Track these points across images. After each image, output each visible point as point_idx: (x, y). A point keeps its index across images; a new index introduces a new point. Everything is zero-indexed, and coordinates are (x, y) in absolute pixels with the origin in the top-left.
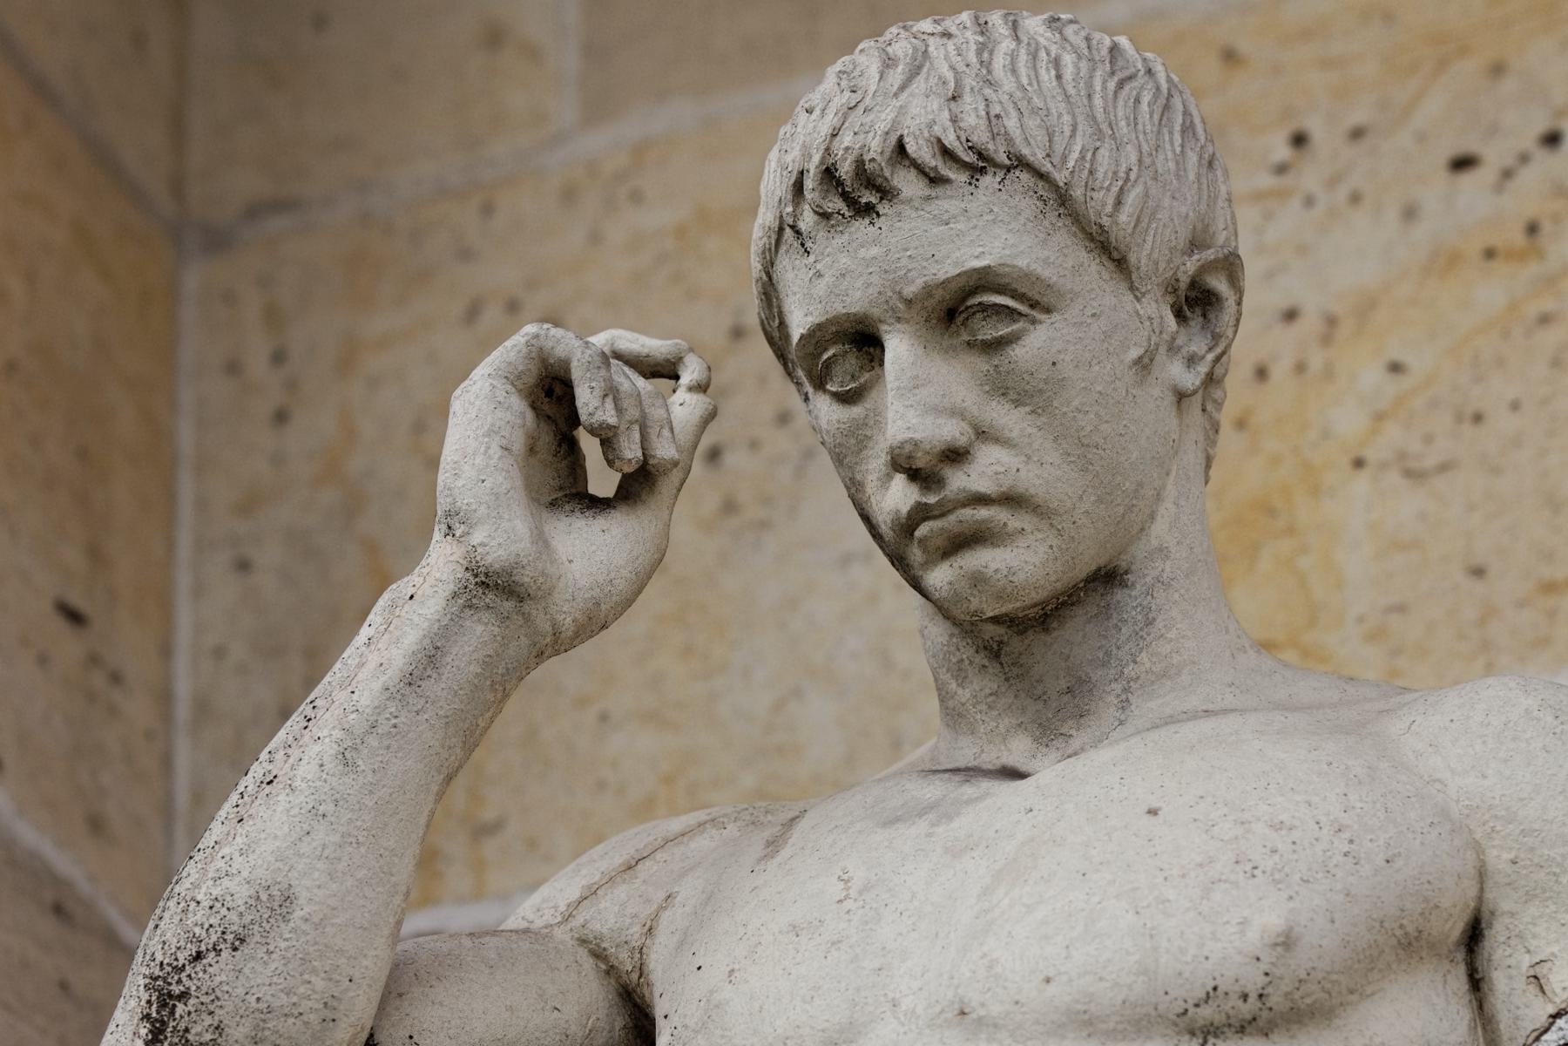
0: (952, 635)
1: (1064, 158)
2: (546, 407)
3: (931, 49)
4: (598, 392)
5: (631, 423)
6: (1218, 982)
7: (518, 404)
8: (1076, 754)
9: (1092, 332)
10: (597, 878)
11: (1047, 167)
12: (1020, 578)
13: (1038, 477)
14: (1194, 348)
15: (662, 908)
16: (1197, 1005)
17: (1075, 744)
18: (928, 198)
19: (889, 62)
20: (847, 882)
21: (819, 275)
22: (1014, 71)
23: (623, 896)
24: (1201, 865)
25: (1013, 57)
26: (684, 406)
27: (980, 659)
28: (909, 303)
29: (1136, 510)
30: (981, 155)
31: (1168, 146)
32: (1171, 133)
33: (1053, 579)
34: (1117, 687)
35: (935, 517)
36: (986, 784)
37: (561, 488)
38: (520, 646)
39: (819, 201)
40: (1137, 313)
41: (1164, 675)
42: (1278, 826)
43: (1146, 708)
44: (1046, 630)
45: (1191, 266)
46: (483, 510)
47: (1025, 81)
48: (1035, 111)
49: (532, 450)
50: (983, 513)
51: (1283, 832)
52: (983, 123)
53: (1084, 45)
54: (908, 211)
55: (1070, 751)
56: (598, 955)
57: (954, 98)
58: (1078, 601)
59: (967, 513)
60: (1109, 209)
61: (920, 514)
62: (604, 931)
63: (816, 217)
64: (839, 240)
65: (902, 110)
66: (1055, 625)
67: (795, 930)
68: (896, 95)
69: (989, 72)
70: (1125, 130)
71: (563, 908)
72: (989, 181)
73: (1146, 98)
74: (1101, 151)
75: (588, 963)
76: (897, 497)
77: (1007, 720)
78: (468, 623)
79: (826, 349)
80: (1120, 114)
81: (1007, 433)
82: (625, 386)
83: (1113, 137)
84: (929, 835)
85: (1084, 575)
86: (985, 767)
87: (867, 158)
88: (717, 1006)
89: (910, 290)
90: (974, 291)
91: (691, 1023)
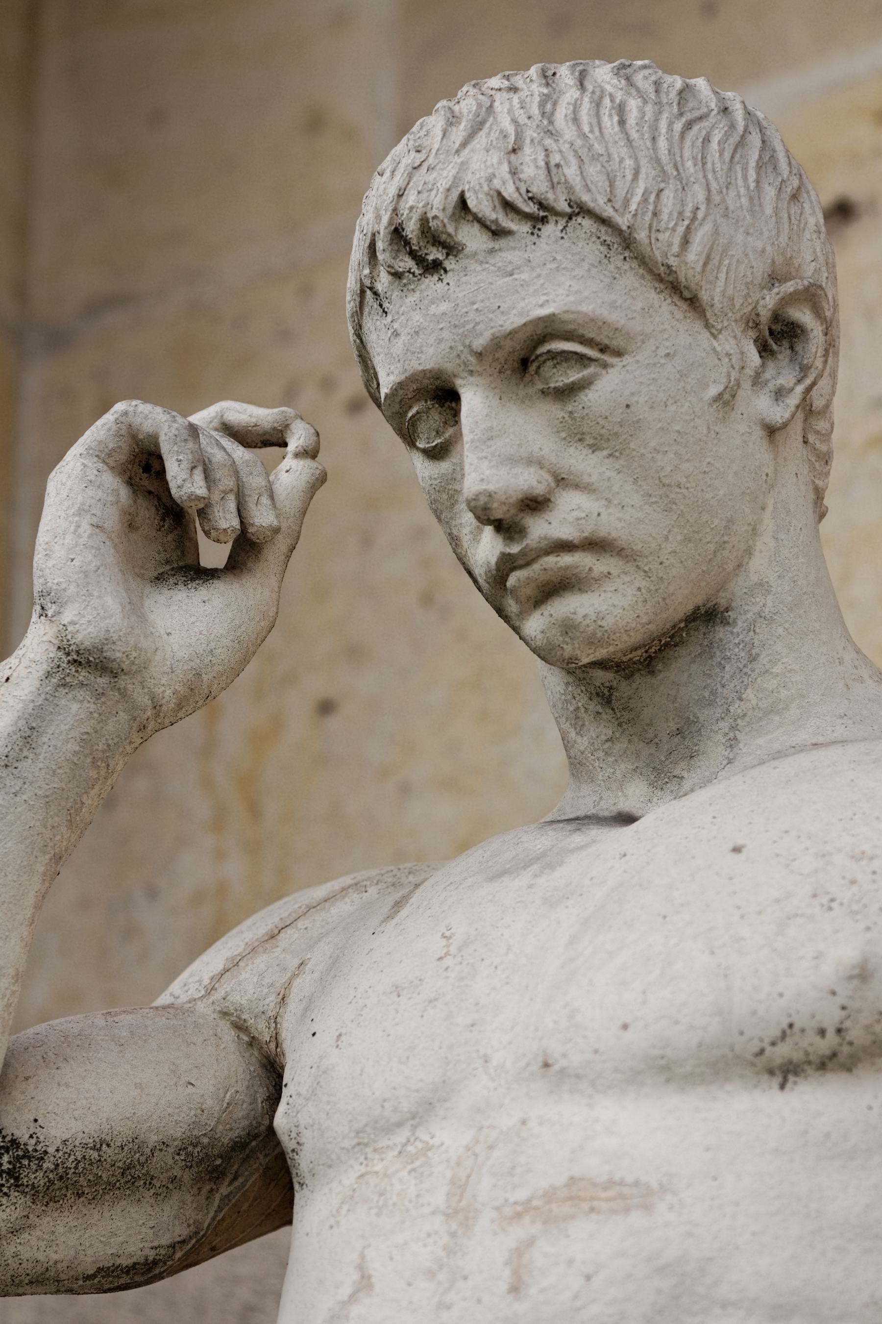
0: (568, 684)
1: (627, 202)
2: (146, 483)
3: (496, 104)
4: (185, 465)
5: (226, 492)
6: (795, 1019)
7: (111, 482)
8: (686, 795)
9: (668, 371)
10: (240, 950)
11: (608, 212)
12: (608, 623)
13: (620, 519)
14: (781, 381)
15: (294, 976)
16: (773, 1044)
17: (686, 785)
18: (492, 251)
19: (453, 120)
20: (448, 938)
21: (396, 334)
22: (576, 120)
23: (262, 966)
24: (777, 901)
25: (576, 107)
26: (290, 473)
27: (594, 706)
28: (480, 355)
29: (728, 546)
30: (541, 205)
31: (740, 182)
32: (745, 170)
33: (644, 620)
34: (724, 725)
35: (521, 567)
36: (595, 832)
37: (167, 562)
38: (119, 723)
39: (391, 261)
40: (714, 349)
41: (772, 710)
42: (858, 857)
43: (753, 745)
44: (652, 673)
45: (770, 301)
46: (72, 589)
47: (586, 129)
48: (595, 158)
49: (131, 526)
50: (566, 560)
51: (864, 862)
52: (543, 173)
53: (651, 89)
54: (473, 266)
55: (681, 794)
56: (240, 1027)
57: (514, 151)
58: (682, 642)
59: (551, 561)
60: (675, 248)
61: (507, 565)
62: (244, 1002)
63: (390, 277)
64: (412, 298)
65: (463, 167)
66: (660, 667)
67: (397, 990)
68: (457, 152)
69: (551, 122)
70: (692, 170)
71: (206, 981)
72: (551, 229)
73: (716, 137)
74: (666, 192)
75: (229, 1035)
76: (487, 548)
77: (623, 766)
78: (63, 702)
79: (410, 407)
80: (687, 154)
81: (586, 479)
82: (218, 456)
83: (679, 178)
84: (530, 887)
85: (681, 615)
86: (601, 814)
87: (430, 215)
88: (324, 1072)
89: (479, 343)
90: (544, 339)
91: (304, 1092)
